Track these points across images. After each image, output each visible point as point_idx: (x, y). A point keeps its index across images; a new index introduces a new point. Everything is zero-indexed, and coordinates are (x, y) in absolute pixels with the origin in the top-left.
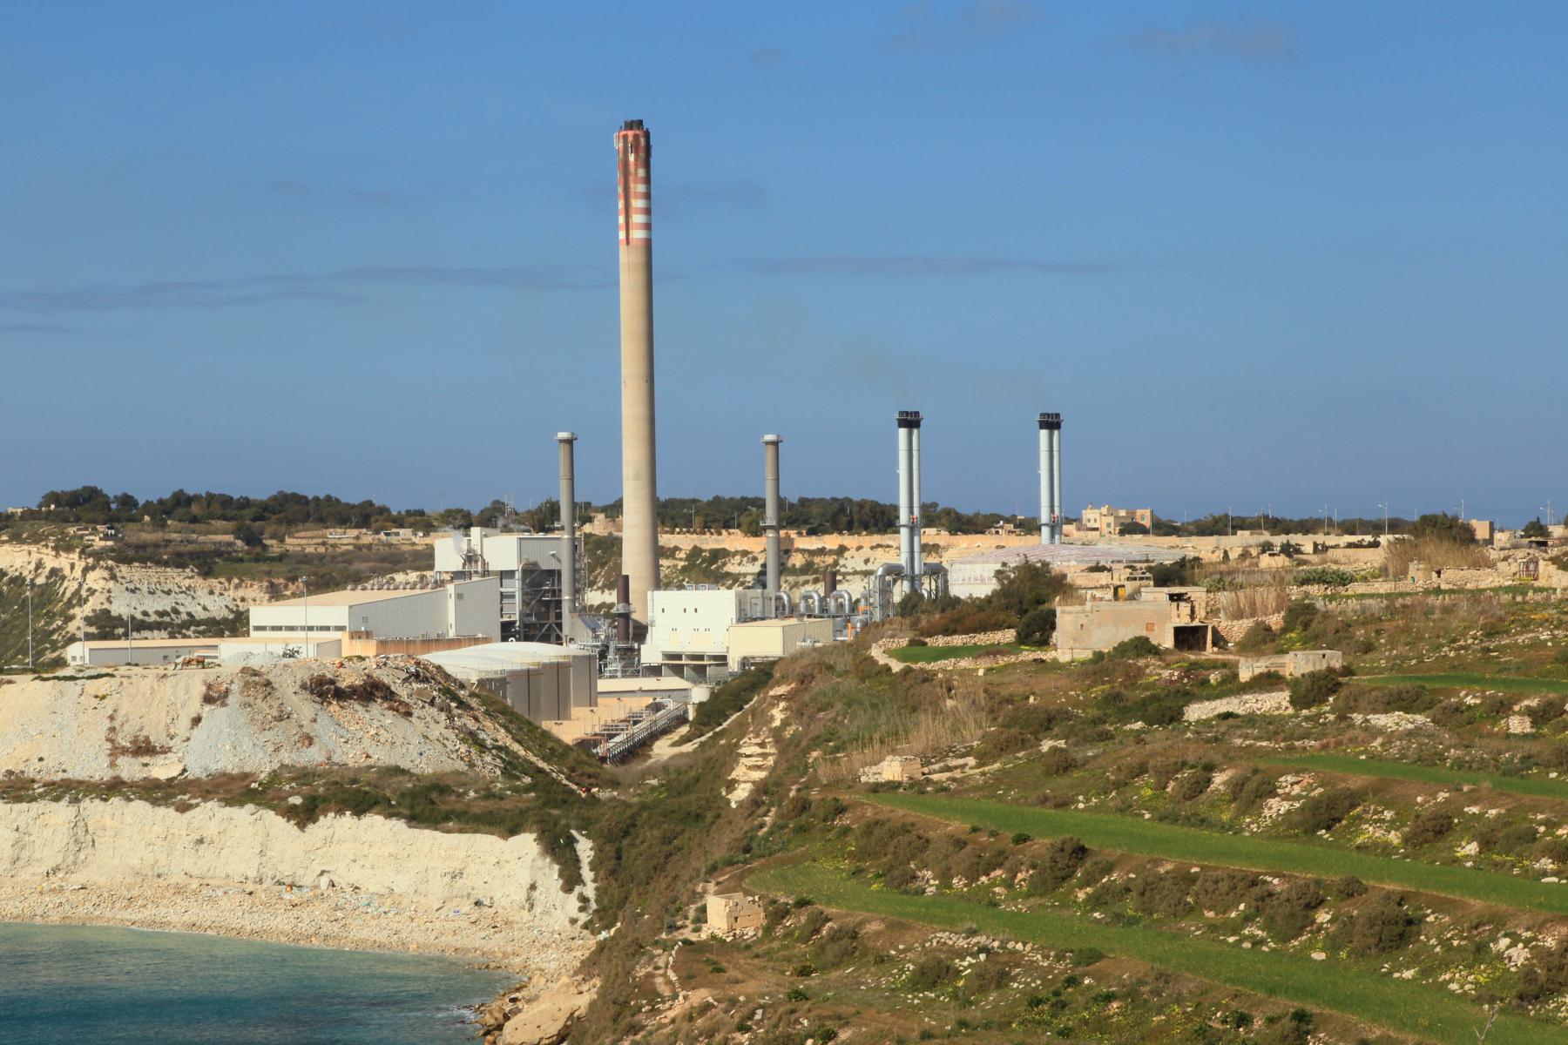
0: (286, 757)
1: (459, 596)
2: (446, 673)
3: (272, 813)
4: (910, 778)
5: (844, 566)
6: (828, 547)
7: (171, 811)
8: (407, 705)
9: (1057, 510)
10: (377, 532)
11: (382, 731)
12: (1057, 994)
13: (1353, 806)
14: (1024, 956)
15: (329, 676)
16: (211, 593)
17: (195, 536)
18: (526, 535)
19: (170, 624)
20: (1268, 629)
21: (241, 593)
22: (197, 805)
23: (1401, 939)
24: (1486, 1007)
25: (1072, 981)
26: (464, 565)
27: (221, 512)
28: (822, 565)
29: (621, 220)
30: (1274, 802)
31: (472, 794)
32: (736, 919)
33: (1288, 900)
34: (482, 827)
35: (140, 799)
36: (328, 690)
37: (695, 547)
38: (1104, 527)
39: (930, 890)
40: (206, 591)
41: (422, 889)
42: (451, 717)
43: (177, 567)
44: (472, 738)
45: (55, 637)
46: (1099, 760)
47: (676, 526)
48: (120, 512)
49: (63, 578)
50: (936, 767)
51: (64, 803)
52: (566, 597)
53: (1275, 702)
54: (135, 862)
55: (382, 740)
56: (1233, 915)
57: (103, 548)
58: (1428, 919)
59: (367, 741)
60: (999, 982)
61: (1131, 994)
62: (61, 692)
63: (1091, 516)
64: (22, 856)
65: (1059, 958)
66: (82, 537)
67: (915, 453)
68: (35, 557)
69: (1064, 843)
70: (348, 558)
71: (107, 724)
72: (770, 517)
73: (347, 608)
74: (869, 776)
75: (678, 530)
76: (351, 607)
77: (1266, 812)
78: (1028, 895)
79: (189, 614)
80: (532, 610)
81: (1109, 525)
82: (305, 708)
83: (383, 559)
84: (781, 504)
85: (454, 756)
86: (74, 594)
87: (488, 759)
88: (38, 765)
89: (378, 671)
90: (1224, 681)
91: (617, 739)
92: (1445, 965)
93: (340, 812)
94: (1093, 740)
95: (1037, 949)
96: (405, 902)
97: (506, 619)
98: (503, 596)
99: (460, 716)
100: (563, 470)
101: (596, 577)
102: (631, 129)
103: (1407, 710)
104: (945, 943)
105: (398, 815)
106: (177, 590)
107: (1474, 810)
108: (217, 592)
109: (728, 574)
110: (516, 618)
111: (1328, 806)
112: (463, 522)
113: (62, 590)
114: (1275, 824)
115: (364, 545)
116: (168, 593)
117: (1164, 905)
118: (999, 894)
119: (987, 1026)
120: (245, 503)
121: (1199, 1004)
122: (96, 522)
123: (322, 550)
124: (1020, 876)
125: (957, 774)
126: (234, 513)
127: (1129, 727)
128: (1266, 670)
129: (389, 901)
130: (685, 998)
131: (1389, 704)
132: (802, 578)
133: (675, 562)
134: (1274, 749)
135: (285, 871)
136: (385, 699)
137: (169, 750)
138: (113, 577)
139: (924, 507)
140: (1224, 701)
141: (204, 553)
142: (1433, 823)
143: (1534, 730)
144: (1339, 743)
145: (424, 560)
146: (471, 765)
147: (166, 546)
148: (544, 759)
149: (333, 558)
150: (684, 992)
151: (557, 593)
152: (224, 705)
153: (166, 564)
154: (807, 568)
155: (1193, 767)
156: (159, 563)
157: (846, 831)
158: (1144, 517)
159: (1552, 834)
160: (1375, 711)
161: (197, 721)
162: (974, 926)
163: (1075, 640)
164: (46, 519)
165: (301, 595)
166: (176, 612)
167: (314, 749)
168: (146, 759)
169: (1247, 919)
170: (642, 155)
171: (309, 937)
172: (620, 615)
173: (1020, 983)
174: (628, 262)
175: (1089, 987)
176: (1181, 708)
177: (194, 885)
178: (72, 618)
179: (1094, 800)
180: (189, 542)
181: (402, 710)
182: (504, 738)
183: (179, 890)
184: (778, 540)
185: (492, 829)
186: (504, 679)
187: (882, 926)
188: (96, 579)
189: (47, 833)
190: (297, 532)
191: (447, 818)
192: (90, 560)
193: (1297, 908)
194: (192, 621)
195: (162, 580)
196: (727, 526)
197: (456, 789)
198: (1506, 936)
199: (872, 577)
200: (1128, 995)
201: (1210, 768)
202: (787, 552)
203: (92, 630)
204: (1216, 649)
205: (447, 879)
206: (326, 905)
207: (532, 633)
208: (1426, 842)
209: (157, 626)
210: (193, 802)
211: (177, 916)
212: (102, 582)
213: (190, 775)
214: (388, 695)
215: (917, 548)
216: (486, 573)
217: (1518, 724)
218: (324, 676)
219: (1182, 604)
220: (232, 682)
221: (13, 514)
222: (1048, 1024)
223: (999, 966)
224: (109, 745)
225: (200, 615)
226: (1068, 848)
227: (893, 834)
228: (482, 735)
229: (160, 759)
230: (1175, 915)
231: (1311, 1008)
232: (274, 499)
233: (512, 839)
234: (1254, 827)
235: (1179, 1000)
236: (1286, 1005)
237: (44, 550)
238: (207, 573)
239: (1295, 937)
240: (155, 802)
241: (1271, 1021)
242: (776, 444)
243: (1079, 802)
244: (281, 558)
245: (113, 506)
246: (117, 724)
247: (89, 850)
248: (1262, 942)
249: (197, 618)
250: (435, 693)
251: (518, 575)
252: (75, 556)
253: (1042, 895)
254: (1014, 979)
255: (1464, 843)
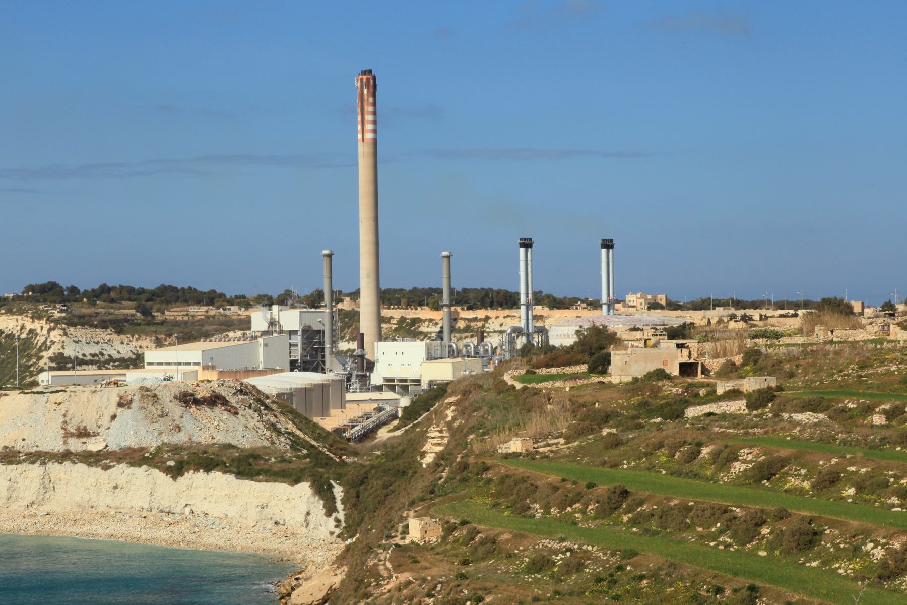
0: (166, 438)
1: (266, 345)
2: (258, 390)
3: (157, 471)
4: (527, 451)
5: (488, 328)
6: (479, 317)
7: (99, 470)
8: (235, 408)
9: (611, 295)
10: (218, 308)
11: (221, 423)
12: (611, 575)
13: (783, 467)
14: (592, 553)
15: (190, 391)
16: (122, 343)
17: (113, 310)
18: (304, 310)
19: (99, 361)
20: (733, 364)
21: (139, 343)
22: (114, 466)
23: (810, 544)
24: (860, 583)
25: (620, 568)
26: (268, 327)
27: (128, 297)
28: (476, 327)
29: (359, 127)
30: (737, 464)
31: (273, 460)
32: (426, 532)
33: (745, 521)
34: (279, 479)
35: (81, 462)
36: (190, 400)
37: (402, 317)
38: (639, 305)
39: (538, 516)
40: (119, 342)
41: (244, 514)
42: (261, 415)
43: (103, 328)
44: (273, 427)
45: (32, 369)
46: (636, 440)
47: (391, 305)
48: (70, 296)
49: (37, 335)
50: (542, 444)
51: (37, 465)
52: (327, 346)
53: (738, 406)
54: (78, 499)
55: (221, 428)
56: (713, 530)
57: (60, 317)
58: (826, 532)
59: (212, 429)
60: (578, 569)
61: (654, 576)
62: (35, 401)
63: (631, 298)
64: (13, 496)
65: (613, 555)
66: (47, 311)
67: (529, 262)
68: (20, 322)
69: (615, 488)
70: (201, 323)
71: (62, 419)
72: (446, 299)
73: (201, 352)
74: (503, 449)
75: (392, 307)
76: (203, 351)
77: (732, 470)
78: (595, 518)
79: (109, 356)
80: (308, 353)
81: (641, 304)
82: (176, 410)
83: (222, 324)
84: (452, 292)
85: (263, 438)
86: (43, 344)
87: (282, 439)
88: (22, 443)
89: (219, 389)
90: (708, 394)
91: (357, 428)
92: (836, 559)
93: (197, 470)
94: (632, 428)
95: (600, 550)
96: (235, 522)
97: (292, 358)
98: (291, 345)
99: (266, 415)
100: (326, 272)
101: (345, 334)
102: (365, 75)
103: (814, 411)
104: (547, 546)
105: (230, 472)
106: (102, 341)
107: (853, 469)
108: (125, 343)
109: (421, 333)
110: (299, 358)
111: (768, 467)
112: (268, 302)
113: (36, 342)
114: (738, 477)
115: (210, 316)
116: (97, 343)
117: (673, 524)
118: (578, 518)
119: (571, 594)
120: (142, 291)
121: (693, 581)
122: (55, 302)
123: (186, 318)
124: (590, 507)
125: (554, 448)
126: (135, 297)
127: (653, 421)
128: (732, 388)
129: (225, 522)
130: (396, 578)
131: (803, 407)
132: (464, 335)
133: (391, 325)
134: (737, 434)
135: (165, 504)
136: (223, 404)
137: (98, 434)
138: (66, 334)
139: (534, 294)
140: (708, 406)
141: (118, 320)
142: (829, 476)
143: (887, 423)
144: (775, 430)
145: (245, 324)
146: (273, 443)
147: (96, 316)
148: (315, 439)
149: (193, 323)
150: (396, 575)
151: (322, 343)
152: (129, 408)
153: (96, 327)
154: (467, 329)
155: (690, 444)
156: (92, 326)
157: (489, 481)
158: (662, 299)
159: (898, 483)
160: (795, 412)
161: (114, 417)
162: (564, 536)
163: (622, 370)
164: (27, 300)
165: (174, 345)
166: (102, 354)
167: (182, 434)
168: (84, 440)
169: (721, 532)
170: (371, 90)
171: (178, 542)
172: (359, 356)
173: (590, 569)
174: (363, 152)
175: (630, 571)
176: (683, 410)
177: (112, 512)
178: (42, 358)
179: (633, 463)
180: (110, 314)
181: (233, 411)
182: (291, 427)
183: (104, 515)
184: (450, 313)
185: (285, 480)
186: (292, 393)
187: (510, 536)
188: (56, 335)
189: (27, 482)
190: (172, 308)
191: (258, 474)
192: (52, 324)
193: (750, 526)
194: (111, 359)
195: (94, 336)
196: (421, 304)
197: (264, 457)
198: (871, 542)
199: (505, 334)
200: (652, 576)
201: (700, 445)
202: (455, 320)
203: (54, 365)
204: (703, 376)
205: (259, 509)
206: (189, 524)
207: (308, 366)
208: (825, 487)
209: (91, 363)
210: (112, 464)
211: (102, 530)
212: (59, 337)
213: (110, 449)
214: (225, 402)
215: (530, 317)
216: (281, 332)
217: (878, 419)
218: (187, 391)
219: (684, 350)
220: (134, 395)
221: (7, 298)
222: (606, 593)
223: (578, 560)
224: (63, 431)
225: (116, 356)
226: (618, 491)
227: (516, 483)
228: (279, 426)
229: (92, 439)
230: (680, 530)
231: (758, 583)
232: (158, 289)
233: (296, 486)
234: (725, 479)
235: (682, 579)
236: (744, 582)
237: (26, 319)
238: (120, 332)
239: (749, 543)
240: (90, 465)
241: (735, 591)
242: (449, 257)
243: (624, 464)
244: (163, 323)
245: (66, 293)
246: (67, 419)
247: (52, 492)
248: (730, 545)
249: (114, 358)
250: (251, 401)
251: (300, 333)
252: (43, 322)
253: (603, 518)
254: (587, 567)
255: (847, 488)
